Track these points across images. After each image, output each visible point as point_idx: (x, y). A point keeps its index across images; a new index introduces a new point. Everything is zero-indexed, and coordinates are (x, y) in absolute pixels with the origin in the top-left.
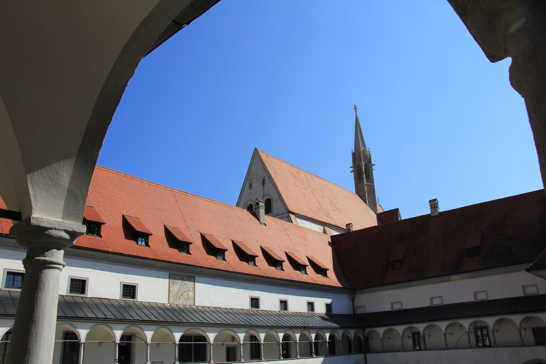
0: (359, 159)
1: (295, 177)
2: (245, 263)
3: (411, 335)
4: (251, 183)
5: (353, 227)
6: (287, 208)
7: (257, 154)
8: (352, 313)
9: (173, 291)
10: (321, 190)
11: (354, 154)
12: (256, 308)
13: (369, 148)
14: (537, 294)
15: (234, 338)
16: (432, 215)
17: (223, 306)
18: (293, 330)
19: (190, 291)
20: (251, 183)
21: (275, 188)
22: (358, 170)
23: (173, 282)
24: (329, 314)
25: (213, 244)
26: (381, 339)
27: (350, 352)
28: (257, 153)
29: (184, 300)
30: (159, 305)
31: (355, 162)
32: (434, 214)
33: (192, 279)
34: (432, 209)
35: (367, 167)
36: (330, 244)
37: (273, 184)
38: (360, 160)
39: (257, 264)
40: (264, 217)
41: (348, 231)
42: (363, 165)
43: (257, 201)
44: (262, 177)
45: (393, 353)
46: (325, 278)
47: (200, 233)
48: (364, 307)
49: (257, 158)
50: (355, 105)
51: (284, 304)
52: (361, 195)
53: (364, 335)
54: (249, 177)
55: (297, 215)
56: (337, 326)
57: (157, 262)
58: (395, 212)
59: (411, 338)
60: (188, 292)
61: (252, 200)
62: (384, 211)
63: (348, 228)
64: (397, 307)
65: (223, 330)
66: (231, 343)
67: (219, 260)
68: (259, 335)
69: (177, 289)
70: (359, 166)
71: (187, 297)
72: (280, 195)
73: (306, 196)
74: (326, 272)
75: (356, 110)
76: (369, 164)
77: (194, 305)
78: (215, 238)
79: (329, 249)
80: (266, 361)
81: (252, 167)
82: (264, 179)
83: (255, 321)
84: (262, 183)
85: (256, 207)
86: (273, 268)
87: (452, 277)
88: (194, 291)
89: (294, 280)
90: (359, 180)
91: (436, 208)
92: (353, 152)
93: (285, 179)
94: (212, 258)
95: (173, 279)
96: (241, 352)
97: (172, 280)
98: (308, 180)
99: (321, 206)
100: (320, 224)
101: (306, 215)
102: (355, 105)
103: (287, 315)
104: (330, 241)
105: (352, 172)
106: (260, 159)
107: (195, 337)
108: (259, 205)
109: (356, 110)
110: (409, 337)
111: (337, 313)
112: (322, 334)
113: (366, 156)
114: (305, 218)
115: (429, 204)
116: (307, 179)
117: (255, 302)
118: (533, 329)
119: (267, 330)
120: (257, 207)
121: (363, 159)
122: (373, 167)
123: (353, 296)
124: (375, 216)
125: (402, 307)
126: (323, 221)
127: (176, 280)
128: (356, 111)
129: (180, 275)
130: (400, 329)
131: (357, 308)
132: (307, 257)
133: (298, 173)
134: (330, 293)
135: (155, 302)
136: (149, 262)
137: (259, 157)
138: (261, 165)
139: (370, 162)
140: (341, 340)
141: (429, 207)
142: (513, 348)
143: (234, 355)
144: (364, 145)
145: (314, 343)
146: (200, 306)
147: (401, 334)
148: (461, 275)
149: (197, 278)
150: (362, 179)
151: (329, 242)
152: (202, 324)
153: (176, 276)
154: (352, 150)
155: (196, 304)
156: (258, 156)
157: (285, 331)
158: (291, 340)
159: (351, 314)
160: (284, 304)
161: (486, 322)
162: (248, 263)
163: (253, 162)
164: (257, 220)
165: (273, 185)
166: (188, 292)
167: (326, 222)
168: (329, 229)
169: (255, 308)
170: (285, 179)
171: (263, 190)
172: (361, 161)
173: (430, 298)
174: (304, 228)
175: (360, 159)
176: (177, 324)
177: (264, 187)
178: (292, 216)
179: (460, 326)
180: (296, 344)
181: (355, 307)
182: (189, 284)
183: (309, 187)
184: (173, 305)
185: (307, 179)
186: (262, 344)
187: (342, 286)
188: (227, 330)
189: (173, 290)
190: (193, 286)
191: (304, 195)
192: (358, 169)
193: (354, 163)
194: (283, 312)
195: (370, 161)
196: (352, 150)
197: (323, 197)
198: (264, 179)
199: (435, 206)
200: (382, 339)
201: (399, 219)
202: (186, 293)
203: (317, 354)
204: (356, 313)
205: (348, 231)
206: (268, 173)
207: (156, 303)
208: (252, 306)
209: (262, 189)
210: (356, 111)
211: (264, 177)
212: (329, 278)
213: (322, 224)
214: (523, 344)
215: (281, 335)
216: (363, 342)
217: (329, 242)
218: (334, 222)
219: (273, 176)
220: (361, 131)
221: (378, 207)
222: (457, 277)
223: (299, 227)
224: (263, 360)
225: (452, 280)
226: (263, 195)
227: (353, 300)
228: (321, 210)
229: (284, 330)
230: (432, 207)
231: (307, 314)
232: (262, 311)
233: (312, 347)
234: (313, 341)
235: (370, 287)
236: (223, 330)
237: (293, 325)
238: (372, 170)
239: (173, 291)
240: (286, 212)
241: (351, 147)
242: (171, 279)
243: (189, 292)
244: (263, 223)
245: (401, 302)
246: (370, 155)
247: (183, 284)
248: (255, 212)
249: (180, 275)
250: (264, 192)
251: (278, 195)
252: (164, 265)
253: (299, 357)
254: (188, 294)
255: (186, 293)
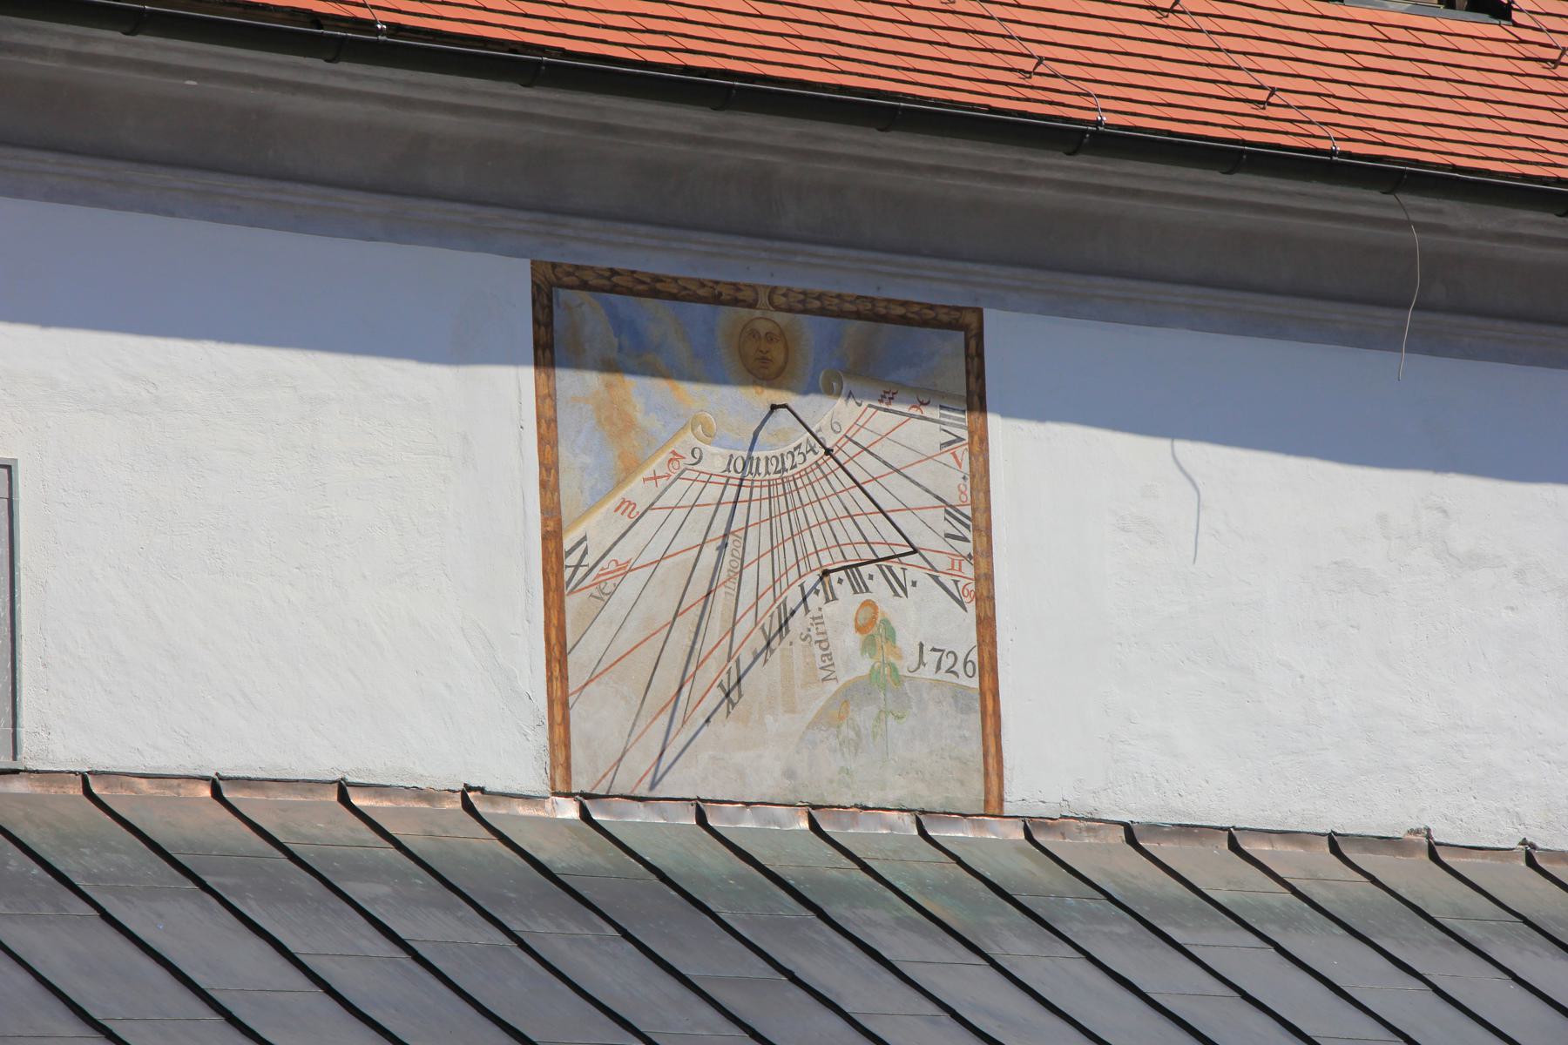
9: (625, 570)
19: (913, 570)
23: (617, 424)
29: (813, 724)
30: (397, 813)
57: (314, 69)
60: (879, 589)
69: (692, 536)
71: (864, 666)
77: (993, 807)
88: (983, 556)
95: (609, 366)
97: (593, 380)
127: (658, 386)
129: (715, 296)
135: (328, 765)
136: (1404, 225)
146: (1093, 822)
153: (656, 316)
184: (641, 815)
189: (622, 553)
190: (952, 481)
207: (343, 791)
239: (625, 570)
242: (577, 362)
243: (900, 588)
247: (783, 438)
249: (716, 300)
252: (438, 122)
254: (873, 628)
255: (847, 602)
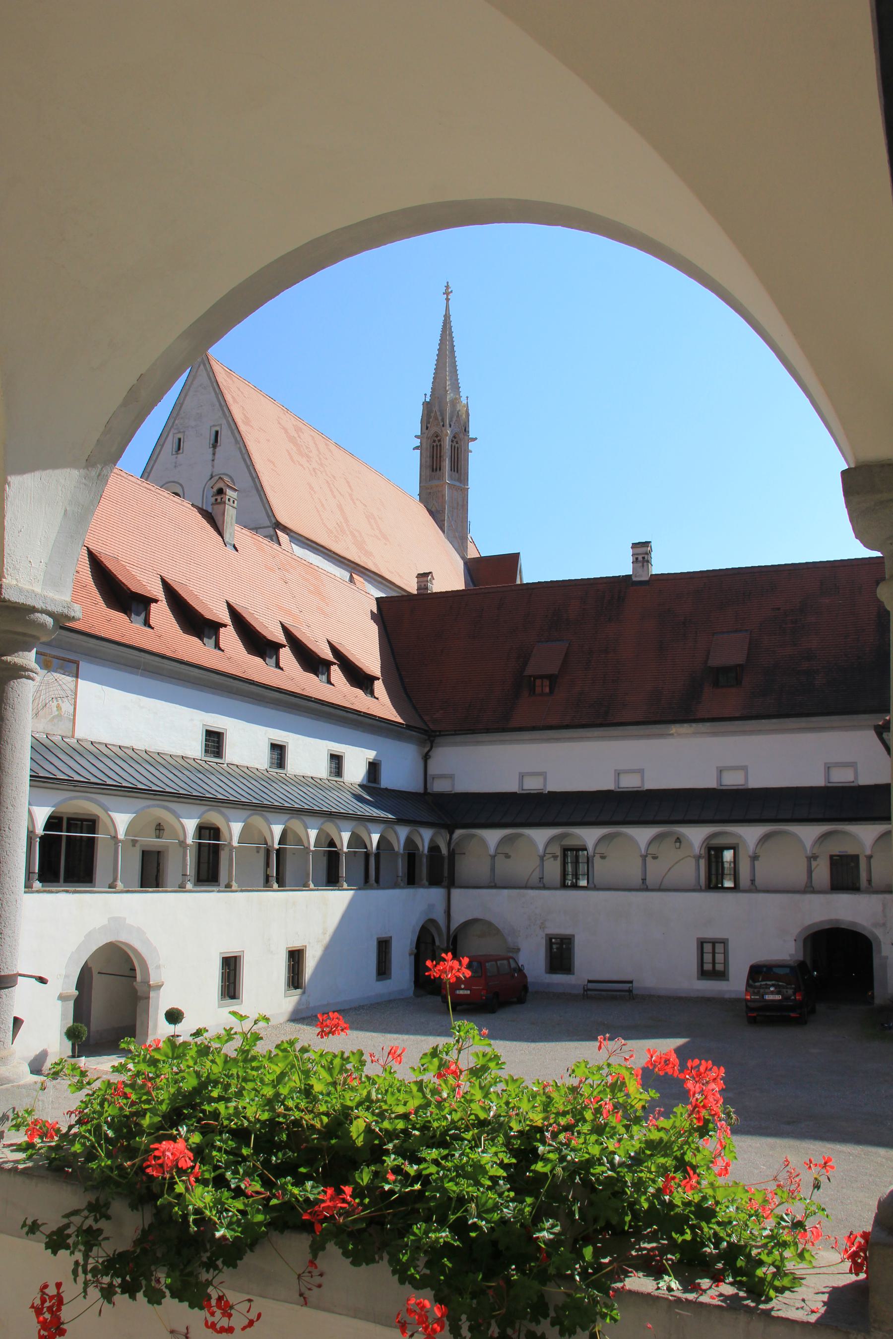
0: (440, 418)
1: (292, 439)
2: (195, 640)
3: (558, 852)
4: (180, 440)
5: (434, 581)
6: (270, 514)
7: (204, 365)
8: (421, 790)
10: (348, 482)
11: (427, 406)
12: (215, 757)
13: (467, 397)
14: (852, 784)
15: (161, 828)
16: (634, 579)
17: (140, 745)
18: (305, 818)
20: (180, 440)
21: (245, 460)
22: (433, 447)
24: (374, 788)
25: (124, 581)
26: (490, 855)
27: (411, 880)
28: (206, 362)
31: (429, 425)
32: (641, 576)
33: (71, 667)
34: (635, 564)
35: (457, 443)
36: (374, 616)
37: (240, 448)
38: (441, 424)
39: (222, 645)
40: (237, 533)
41: (422, 591)
42: (447, 435)
43: (220, 485)
44: (214, 426)
45: (518, 891)
46: (369, 698)
47: (86, 548)
48: (451, 777)
49: (204, 374)
50: (448, 283)
51: (278, 751)
52: (433, 510)
53: (449, 844)
54: (177, 422)
55: (295, 535)
56: (390, 816)
58: (510, 562)
59: (559, 859)
60: (60, 702)
61: (178, 483)
62: (481, 557)
63: (423, 584)
64: (533, 785)
65: (71, 799)
66: (151, 841)
67: (135, 623)
68: (229, 827)
70: (437, 436)
71: (57, 713)
72: (256, 480)
73: (314, 491)
74: (372, 683)
75: (447, 296)
76: (461, 436)
77: (73, 737)
78: (123, 565)
79: (373, 630)
80: (242, 891)
81: (188, 397)
82: (217, 432)
83: (215, 788)
84: (211, 443)
85: (216, 500)
86: (258, 660)
87: (674, 729)
88: (75, 698)
89: (307, 696)
90: (433, 471)
91: (645, 564)
92: (428, 400)
93: (268, 441)
94: (119, 617)
96: (187, 865)
98: (320, 453)
99: (346, 521)
100: (344, 567)
101: (314, 539)
102: (448, 283)
103: (285, 781)
104: (375, 611)
105: (416, 448)
106: (213, 380)
107: (69, 819)
108: (226, 494)
109: (447, 296)
110: (553, 857)
111: (390, 787)
112: (364, 836)
113: (458, 416)
114: (311, 546)
115: (630, 551)
116: (318, 450)
117: (213, 741)
118: (831, 857)
119: (287, 817)
120: (219, 500)
121: (451, 421)
122: (472, 445)
123: (426, 749)
124: (461, 564)
125: (545, 785)
126: (352, 559)
128: (448, 300)
130: (540, 836)
131: (433, 778)
132: (328, 641)
133: (298, 430)
134: (378, 735)
137: (211, 374)
138: (213, 394)
139: (465, 430)
140: (401, 851)
141: (631, 559)
142: (790, 895)
143: (158, 871)
144: (456, 388)
145: (346, 853)
146: (86, 740)
147: (541, 847)
148: (694, 725)
149: (83, 665)
150: (440, 469)
151: (372, 612)
152: (103, 788)
154: (426, 395)
155: (76, 736)
156: (206, 370)
157: (286, 821)
158: (288, 843)
159: (418, 791)
160: (278, 751)
161: (740, 837)
162: (201, 639)
163: (192, 383)
164: (215, 533)
165: (241, 452)
166: (60, 702)
167: (358, 561)
168: (361, 580)
169: (212, 755)
170: (268, 441)
171: (213, 460)
172: (443, 426)
173: (615, 770)
174: (320, 570)
175: (443, 420)
176: (45, 782)
177: (214, 454)
178: (283, 536)
179: (676, 842)
180: (308, 853)
181: (428, 776)
182: (64, 681)
183: (322, 469)
185: (318, 450)
186: (235, 848)
187: (401, 721)
188: (159, 806)
190: (73, 687)
191: (311, 488)
192: (435, 444)
193: (427, 428)
194: (274, 771)
195: (466, 430)
196: (426, 395)
197: (352, 500)
198: (217, 432)
199: (643, 558)
200: (493, 857)
201: (518, 582)
202: (55, 703)
203: (332, 880)
204: (429, 791)
205: (422, 591)
206: (230, 419)
208: (206, 751)
209: (210, 457)
210: (448, 300)
211: (217, 428)
212: (377, 699)
213: (348, 565)
214: (809, 889)
215: (190, 825)
216: (424, 860)
217: (372, 612)
218: (375, 564)
219: (242, 428)
220: (453, 351)
221: (470, 545)
222: (685, 728)
223: (308, 564)
224: (233, 888)
225: (672, 734)
226: (210, 474)
227: (426, 758)
228: (348, 533)
229: (199, 809)
230: (637, 559)
231: (327, 782)
232: (229, 765)
233: (271, 860)
234: (276, 846)
235: (473, 731)
236: (149, 807)
237: (307, 807)
238: (468, 451)
240: (268, 524)
241: (424, 388)
243: (63, 702)
244: (230, 544)
245: (543, 775)
246: (468, 415)
248: (211, 513)
250: (213, 466)
251: (250, 479)
253: (312, 886)
254: (58, 707)
